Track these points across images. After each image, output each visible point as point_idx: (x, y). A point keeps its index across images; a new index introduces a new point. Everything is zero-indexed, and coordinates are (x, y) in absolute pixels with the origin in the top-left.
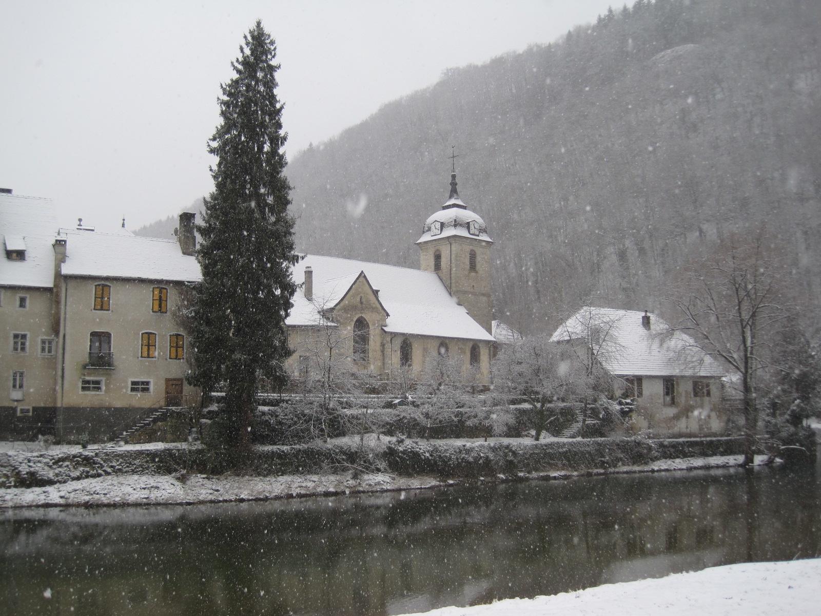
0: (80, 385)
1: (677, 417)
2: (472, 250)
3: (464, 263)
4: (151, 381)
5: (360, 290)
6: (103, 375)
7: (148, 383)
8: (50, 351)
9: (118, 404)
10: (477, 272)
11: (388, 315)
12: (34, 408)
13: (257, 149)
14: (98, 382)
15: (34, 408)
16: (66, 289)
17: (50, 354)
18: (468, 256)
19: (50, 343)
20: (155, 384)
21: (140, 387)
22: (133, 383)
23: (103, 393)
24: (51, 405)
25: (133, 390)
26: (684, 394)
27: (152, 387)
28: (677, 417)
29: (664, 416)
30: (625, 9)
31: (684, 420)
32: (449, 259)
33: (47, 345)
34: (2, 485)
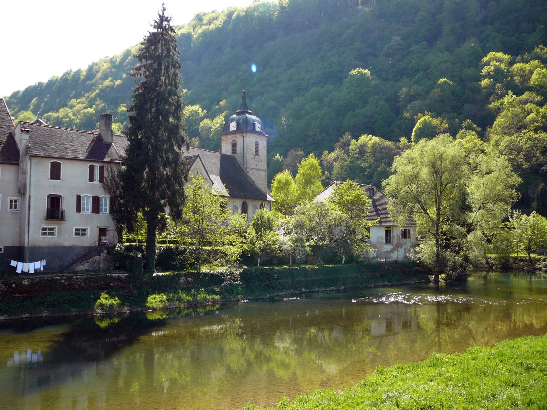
0: (41, 231)
1: (392, 251)
2: (257, 142)
3: (251, 150)
4: (89, 228)
5: (197, 167)
6: (56, 224)
7: (85, 230)
8: (15, 207)
9: (67, 244)
10: (259, 156)
11: (213, 183)
12: (4, 247)
13: (33, 99)
14: (52, 229)
15: (4, 247)
16: (31, 164)
17: (15, 209)
18: (254, 145)
19: (16, 201)
20: (91, 231)
21: (81, 232)
22: (76, 230)
23: (56, 237)
24: (16, 244)
25: (76, 234)
26: (396, 236)
27: (88, 232)
28: (392, 251)
29: (385, 250)
30: (282, 8)
31: (396, 253)
32: (242, 147)
33: (13, 203)
34: (546, 368)
